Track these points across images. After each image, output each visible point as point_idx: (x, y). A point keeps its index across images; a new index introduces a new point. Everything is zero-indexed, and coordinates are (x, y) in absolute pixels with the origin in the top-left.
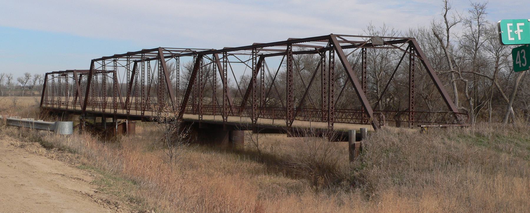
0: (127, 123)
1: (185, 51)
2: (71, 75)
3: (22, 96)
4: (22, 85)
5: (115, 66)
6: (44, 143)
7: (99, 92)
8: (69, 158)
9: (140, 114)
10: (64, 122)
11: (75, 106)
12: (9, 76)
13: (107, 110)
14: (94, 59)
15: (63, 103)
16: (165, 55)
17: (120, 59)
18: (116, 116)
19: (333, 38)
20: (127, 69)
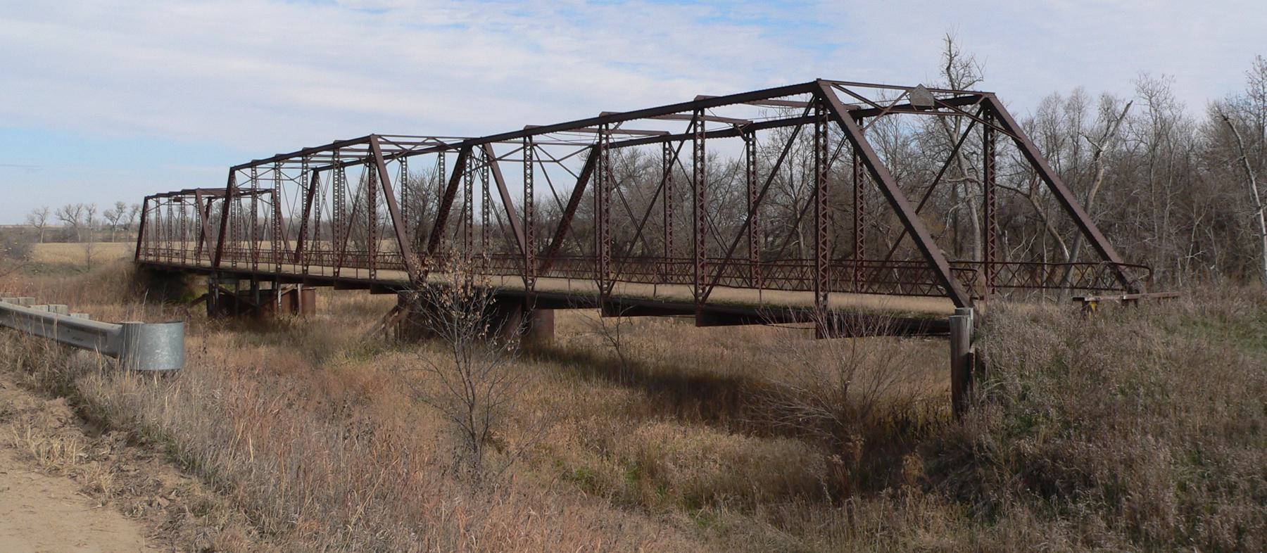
0: (299, 291)
1: (423, 143)
2: (190, 200)
3: (111, 241)
4: (112, 224)
5: (278, 180)
6: (82, 406)
8: (167, 503)
9: (331, 275)
10: (154, 326)
11: (198, 258)
13: (262, 267)
14: (235, 167)
15: (177, 254)
16: (384, 154)
17: (286, 165)
18: (279, 278)
19: (824, 88)
20: (303, 187)
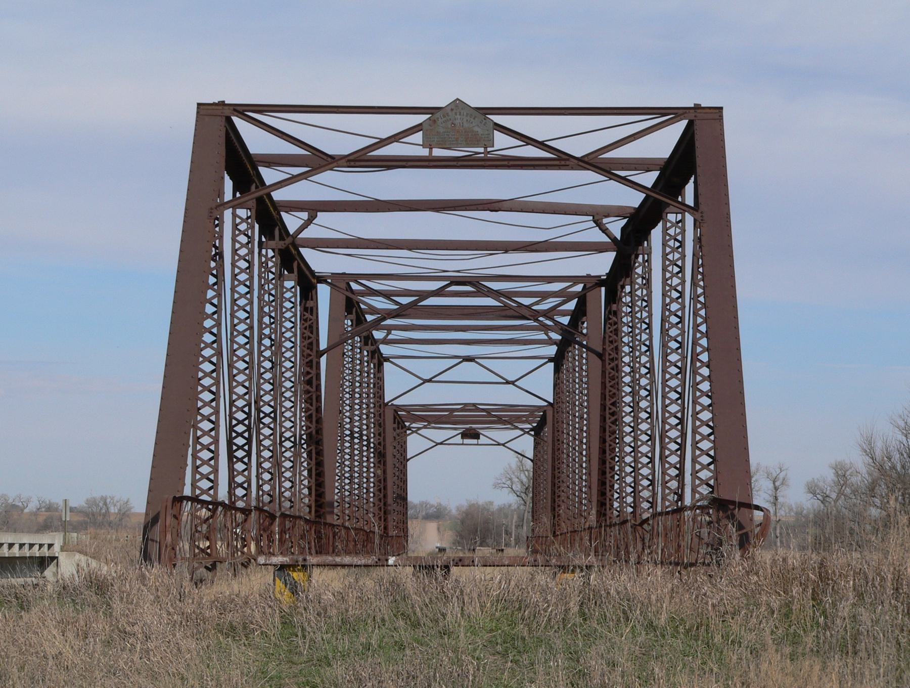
7: (640, 537)
12: (774, 475)
